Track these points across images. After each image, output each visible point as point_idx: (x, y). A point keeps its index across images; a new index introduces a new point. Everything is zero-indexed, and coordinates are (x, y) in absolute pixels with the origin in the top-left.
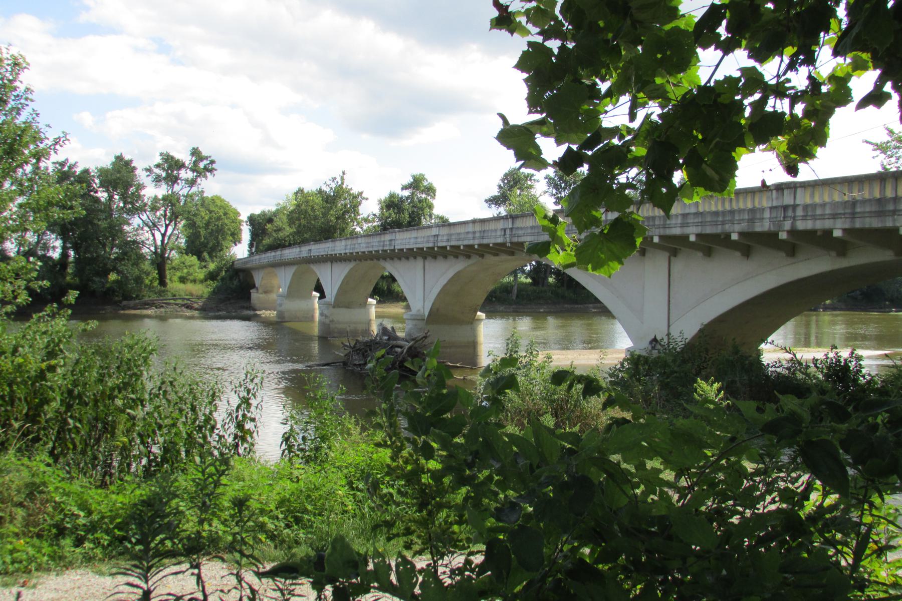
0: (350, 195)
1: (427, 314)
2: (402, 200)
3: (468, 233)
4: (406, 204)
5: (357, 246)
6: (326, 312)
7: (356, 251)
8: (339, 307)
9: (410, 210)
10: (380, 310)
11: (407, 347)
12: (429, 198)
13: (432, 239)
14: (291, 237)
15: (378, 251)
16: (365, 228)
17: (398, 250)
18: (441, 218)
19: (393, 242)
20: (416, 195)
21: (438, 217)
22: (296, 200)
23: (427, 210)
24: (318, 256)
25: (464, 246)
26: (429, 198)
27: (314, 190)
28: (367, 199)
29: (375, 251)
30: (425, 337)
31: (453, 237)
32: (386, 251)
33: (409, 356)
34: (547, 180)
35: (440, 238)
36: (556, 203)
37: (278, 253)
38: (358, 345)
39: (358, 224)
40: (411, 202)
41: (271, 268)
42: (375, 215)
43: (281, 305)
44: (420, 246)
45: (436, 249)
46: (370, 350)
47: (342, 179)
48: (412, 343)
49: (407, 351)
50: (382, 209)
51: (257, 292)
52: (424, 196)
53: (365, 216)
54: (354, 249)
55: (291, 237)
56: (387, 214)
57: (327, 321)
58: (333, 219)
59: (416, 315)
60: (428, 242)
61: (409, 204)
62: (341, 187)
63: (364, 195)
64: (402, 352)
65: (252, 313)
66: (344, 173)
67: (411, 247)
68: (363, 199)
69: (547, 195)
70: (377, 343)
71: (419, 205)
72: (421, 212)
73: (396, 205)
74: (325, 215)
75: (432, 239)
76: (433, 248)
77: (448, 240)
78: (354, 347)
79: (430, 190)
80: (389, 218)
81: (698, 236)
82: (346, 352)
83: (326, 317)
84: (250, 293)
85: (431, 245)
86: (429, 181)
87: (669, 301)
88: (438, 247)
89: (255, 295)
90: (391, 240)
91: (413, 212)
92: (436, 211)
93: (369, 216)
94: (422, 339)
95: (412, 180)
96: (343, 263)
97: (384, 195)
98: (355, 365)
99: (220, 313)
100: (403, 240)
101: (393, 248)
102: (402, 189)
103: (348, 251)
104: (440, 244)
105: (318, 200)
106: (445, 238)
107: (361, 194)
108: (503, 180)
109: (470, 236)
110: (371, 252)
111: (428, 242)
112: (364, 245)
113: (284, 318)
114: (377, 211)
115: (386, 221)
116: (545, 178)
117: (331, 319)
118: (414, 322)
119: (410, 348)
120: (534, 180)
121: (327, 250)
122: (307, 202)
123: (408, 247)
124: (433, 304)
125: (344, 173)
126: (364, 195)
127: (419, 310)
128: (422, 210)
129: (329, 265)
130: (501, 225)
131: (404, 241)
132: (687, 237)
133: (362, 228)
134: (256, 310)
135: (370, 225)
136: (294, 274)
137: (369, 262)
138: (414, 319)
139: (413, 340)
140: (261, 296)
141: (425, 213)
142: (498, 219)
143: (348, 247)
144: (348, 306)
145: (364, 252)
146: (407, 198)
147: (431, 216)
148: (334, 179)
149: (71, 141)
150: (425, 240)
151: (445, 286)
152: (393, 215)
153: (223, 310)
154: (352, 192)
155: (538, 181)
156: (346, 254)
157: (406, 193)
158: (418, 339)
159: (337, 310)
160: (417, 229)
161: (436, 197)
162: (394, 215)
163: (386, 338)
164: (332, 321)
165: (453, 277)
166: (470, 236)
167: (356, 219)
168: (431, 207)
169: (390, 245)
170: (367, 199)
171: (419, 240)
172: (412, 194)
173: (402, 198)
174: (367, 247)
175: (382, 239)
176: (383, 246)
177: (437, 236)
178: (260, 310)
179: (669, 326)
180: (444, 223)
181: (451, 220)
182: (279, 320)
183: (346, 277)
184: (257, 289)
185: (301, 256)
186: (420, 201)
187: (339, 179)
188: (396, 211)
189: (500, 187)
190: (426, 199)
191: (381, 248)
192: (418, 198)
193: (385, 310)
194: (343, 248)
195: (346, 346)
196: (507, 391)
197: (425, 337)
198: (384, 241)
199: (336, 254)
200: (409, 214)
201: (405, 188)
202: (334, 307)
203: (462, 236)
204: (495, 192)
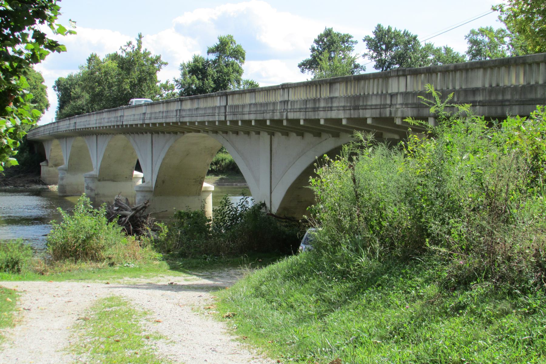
2: (206, 64)
4: (211, 71)
6: (91, 185)
8: (104, 180)
18: (251, 84)
21: (247, 82)
23: (233, 76)
24: (131, 125)
25: (198, 122)
28: (166, 64)
34: (366, 42)
36: (376, 67)
37: (73, 121)
41: (79, 138)
42: (177, 81)
43: (62, 179)
47: (140, 43)
50: (184, 75)
51: (47, 165)
52: (231, 60)
53: (164, 82)
54: (100, 123)
58: (127, 87)
62: (137, 53)
65: (39, 187)
66: (140, 36)
68: (162, 64)
69: (366, 58)
72: (227, 78)
73: (201, 70)
74: (120, 82)
79: (238, 54)
81: (326, 120)
83: (92, 190)
84: (40, 167)
86: (237, 43)
87: (271, 172)
89: (44, 169)
90: (121, 116)
92: (244, 77)
94: (141, 209)
95: (219, 43)
97: (188, 59)
99: (8, 187)
102: (209, 52)
105: (114, 65)
107: (158, 58)
108: (317, 42)
112: (106, 120)
113: (65, 192)
114: (178, 75)
116: (364, 41)
117: (96, 192)
120: (352, 42)
121: (85, 123)
125: (140, 36)
128: (228, 76)
129: (95, 137)
130: (302, 95)
132: (319, 120)
134: (48, 185)
138: (142, 191)
140: (51, 169)
142: (307, 85)
143: (148, 116)
144: (114, 179)
147: (238, 82)
148: (129, 44)
152: (196, 83)
153: (11, 184)
155: (356, 42)
157: (213, 57)
159: (100, 184)
162: (197, 82)
164: (97, 195)
168: (239, 72)
170: (166, 64)
171: (136, 117)
173: (207, 62)
174: (108, 122)
178: (50, 185)
179: (271, 193)
180: (253, 89)
181: (261, 85)
182: (61, 194)
184: (47, 162)
187: (135, 43)
188: (200, 76)
189: (313, 50)
191: (115, 124)
201: (210, 51)
202: (99, 180)
204: (308, 56)
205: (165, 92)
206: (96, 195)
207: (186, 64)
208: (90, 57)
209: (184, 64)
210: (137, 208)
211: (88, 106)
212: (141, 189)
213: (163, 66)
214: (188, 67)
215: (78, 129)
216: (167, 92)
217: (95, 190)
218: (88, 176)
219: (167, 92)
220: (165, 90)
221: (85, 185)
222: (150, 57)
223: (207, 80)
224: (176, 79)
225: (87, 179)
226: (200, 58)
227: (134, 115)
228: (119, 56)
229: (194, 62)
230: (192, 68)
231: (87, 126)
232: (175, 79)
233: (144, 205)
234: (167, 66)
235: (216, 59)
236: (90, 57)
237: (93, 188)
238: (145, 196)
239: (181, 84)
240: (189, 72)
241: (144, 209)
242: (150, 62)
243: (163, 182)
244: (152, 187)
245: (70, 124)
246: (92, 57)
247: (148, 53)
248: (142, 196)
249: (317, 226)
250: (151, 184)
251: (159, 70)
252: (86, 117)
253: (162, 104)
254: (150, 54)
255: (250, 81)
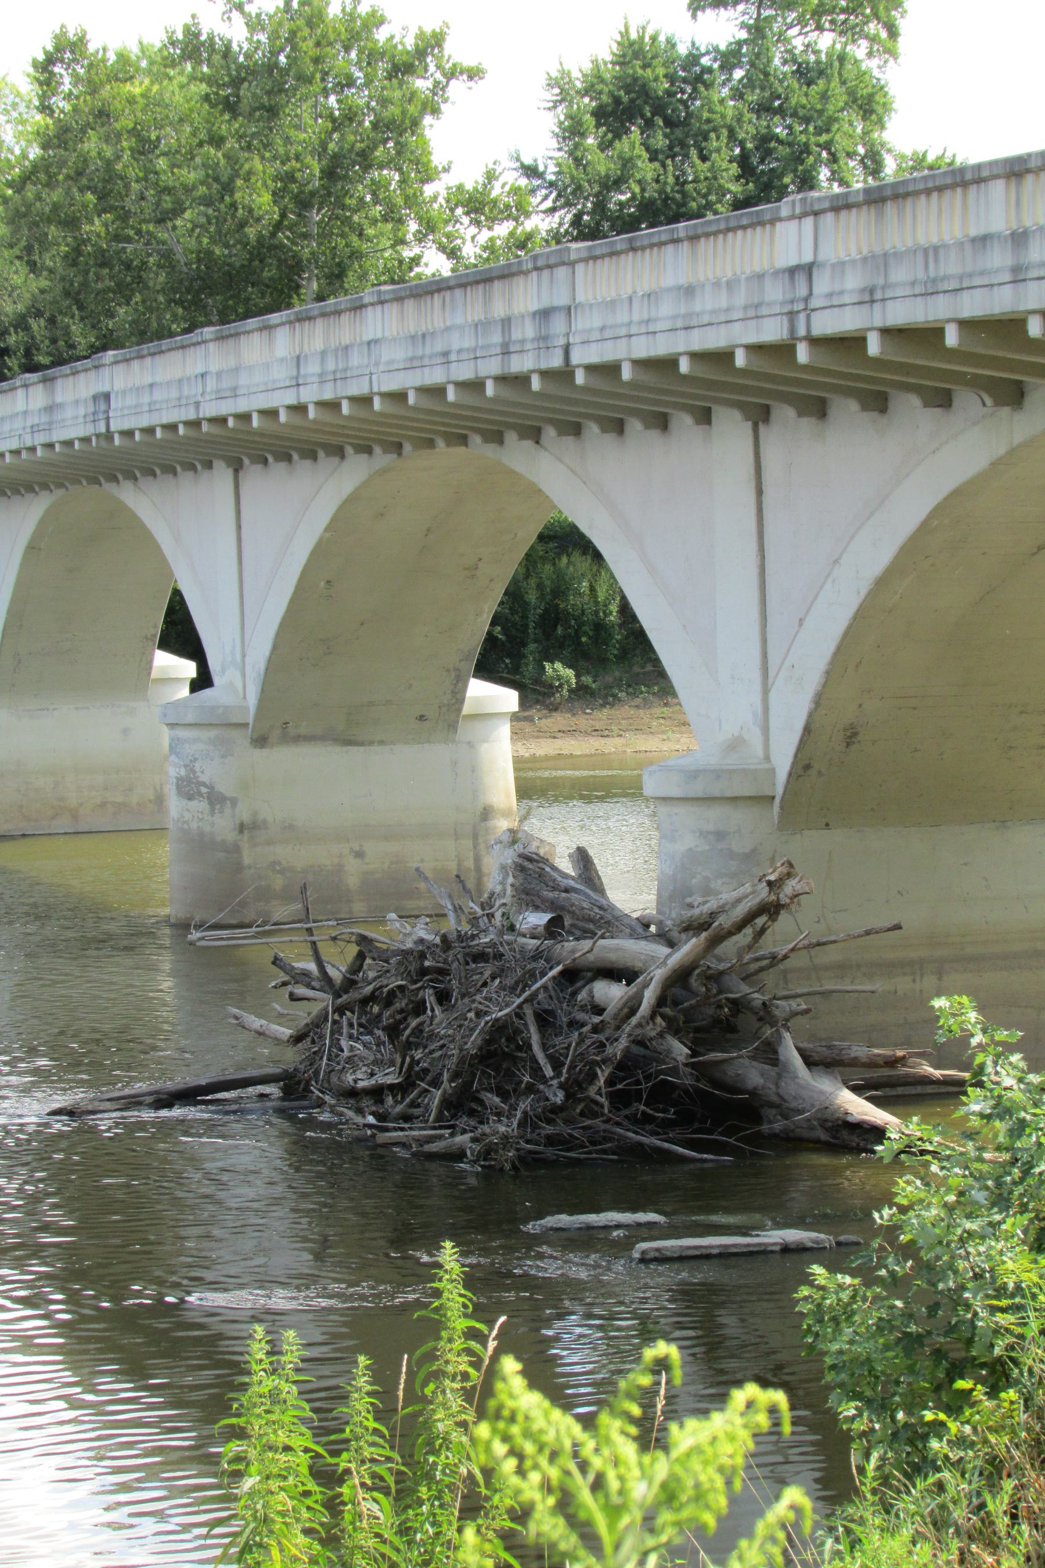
0: (372, 56)
1: (783, 763)
3: (983, 240)
5: (356, 359)
6: (210, 772)
7: (357, 388)
8: (291, 737)
9: (747, 131)
10: (544, 748)
11: (659, 974)
12: (859, 50)
13: (775, 292)
14: (37, 326)
15: (476, 386)
16: (470, 251)
17: (591, 369)
19: (558, 325)
20: (782, 39)
22: (45, 109)
26: (859, 50)
27: (156, 39)
28: (474, 74)
29: (462, 385)
30: (771, 910)
31: (900, 274)
32: (520, 381)
33: (674, 1029)
35: (822, 285)
38: (370, 969)
39: (429, 227)
40: (749, 82)
42: (531, 171)
44: (713, 340)
45: (803, 354)
46: (443, 997)
48: (689, 947)
49: (661, 1001)
52: (826, 41)
53: (471, 178)
54: (340, 377)
55: (37, 326)
56: (602, 164)
57: (223, 826)
59: (718, 774)
60: (755, 312)
61: (738, 95)
63: (455, 51)
64: (631, 1007)
67: (660, 348)
68: (451, 75)
70: (480, 957)
71: (799, 96)
75: (775, 292)
76: (783, 351)
77: (870, 297)
78: (349, 984)
80: (618, 183)
82: (303, 1014)
83: (216, 800)
85: (772, 331)
87: (764, 642)
88: (815, 342)
90: (545, 314)
91: (765, 140)
93: (491, 177)
94: (748, 920)
96: (304, 466)
98: (352, 1093)
100: (611, 305)
101: (556, 362)
103: (309, 395)
104: (826, 324)
106: (853, 282)
109: (999, 259)
110: (437, 392)
111: (755, 312)
112: (398, 354)
115: (600, 207)
117: (244, 813)
118: (714, 817)
119: (681, 977)
121: (193, 391)
122: (103, 115)
123: (644, 349)
124: (818, 700)
126: (455, 51)
127: (735, 744)
129: (222, 477)
131: (622, 316)
133: (453, 254)
135: (503, 229)
136: (32, 548)
137: (445, 455)
139: (693, 927)
141: (841, 143)
143: (312, 368)
145: (399, 397)
146: (729, 59)
149: (641, 22)
150: (741, 298)
151: (882, 582)
154: (381, 35)
156: (299, 409)
158: (724, 921)
160: (694, 238)
161: (903, 43)
162: (647, 169)
163: (538, 919)
165: (924, 528)
166: (999, 259)
167: (412, 201)
169: (543, 340)
170: (474, 74)
171: (706, 303)
172: (758, 30)
173: (693, 59)
174: (412, 364)
175: (499, 310)
176: (506, 352)
177: (808, 270)
183: (319, 553)
185: (59, 435)
186: (806, 74)
188: (660, 141)
190: (842, 58)
191: (491, 367)
192: (791, 57)
193: (610, 745)
194: (282, 374)
195: (303, 978)
196: (448, 1244)
197: (771, 910)
198: (506, 323)
199: (244, 417)
200: (743, 161)
202: (261, 741)
203: (951, 266)
205: (473, 230)
206: (242, 828)
207: (576, 74)
208: (50, 48)
209: (565, 74)
210: (713, 915)
211: (27, 328)
212: (697, 789)
213: (456, 88)
214: (586, 92)
215: (128, 434)
216: (484, 236)
217: (234, 802)
218: (190, 718)
219: (484, 236)
220: (477, 223)
221: (174, 771)
222: (381, 35)
223: (704, 159)
224: (528, 161)
225: (182, 733)
226: (654, 39)
227: (689, 291)
228: (211, 38)
229: (622, 61)
230: (611, 94)
231: (210, 409)
232: (518, 159)
233: (763, 893)
234: (478, 86)
235: (740, 44)
236: (50, 48)
237: (225, 787)
238: (720, 835)
239: (552, 185)
240: (600, 114)
241: (760, 921)
242: (382, 67)
243: (851, 736)
244: (772, 771)
245: (50, 409)
246: (59, 49)
247: (373, 14)
248: (703, 834)
249: (502, 825)
250: (760, 752)
251: (435, 111)
252: (200, 350)
253: (923, 197)
254: (382, 22)
255: (931, 158)
